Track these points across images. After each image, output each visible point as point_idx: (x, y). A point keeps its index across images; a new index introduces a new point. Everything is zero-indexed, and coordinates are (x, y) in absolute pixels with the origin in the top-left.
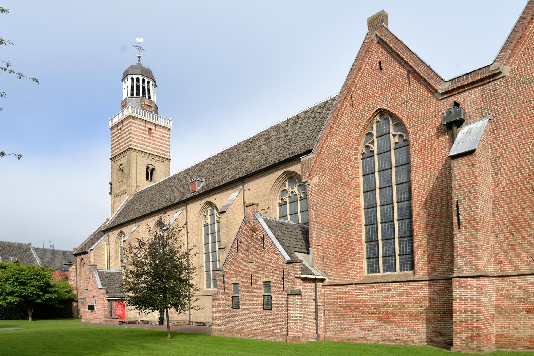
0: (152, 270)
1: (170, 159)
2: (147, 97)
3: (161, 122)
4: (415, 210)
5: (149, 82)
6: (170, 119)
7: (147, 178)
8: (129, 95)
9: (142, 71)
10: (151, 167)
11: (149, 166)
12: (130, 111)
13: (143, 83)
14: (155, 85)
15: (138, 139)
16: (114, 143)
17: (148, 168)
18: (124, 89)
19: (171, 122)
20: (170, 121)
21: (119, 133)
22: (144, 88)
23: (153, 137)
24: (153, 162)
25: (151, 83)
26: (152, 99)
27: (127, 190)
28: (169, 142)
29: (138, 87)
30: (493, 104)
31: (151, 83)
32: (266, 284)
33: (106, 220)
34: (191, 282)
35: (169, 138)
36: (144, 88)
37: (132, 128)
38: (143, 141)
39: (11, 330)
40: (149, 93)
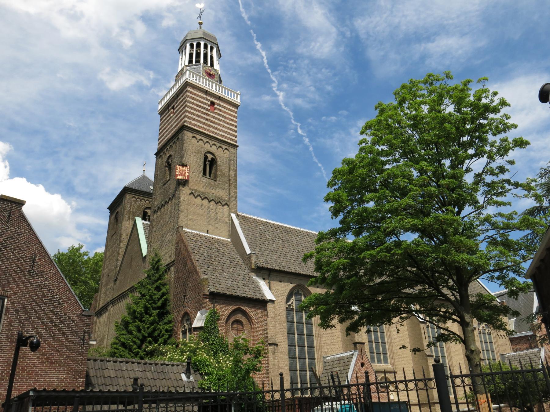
0: (434, 164)
1: (237, 146)
2: (209, 64)
4: (14, 342)
5: (212, 48)
6: (238, 92)
7: (205, 173)
8: (187, 63)
9: (203, 35)
10: (210, 157)
12: (187, 77)
13: (204, 48)
15: (197, 106)
16: (163, 122)
17: (206, 158)
18: (180, 60)
19: (239, 96)
22: (205, 55)
24: (213, 149)
25: (215, 51)
28: (236, 136)
29: (198, 55)
30: (20, 374)
31: (215, 51)
32: (290, 323)
36: (205, 55)
37: (187, 119)
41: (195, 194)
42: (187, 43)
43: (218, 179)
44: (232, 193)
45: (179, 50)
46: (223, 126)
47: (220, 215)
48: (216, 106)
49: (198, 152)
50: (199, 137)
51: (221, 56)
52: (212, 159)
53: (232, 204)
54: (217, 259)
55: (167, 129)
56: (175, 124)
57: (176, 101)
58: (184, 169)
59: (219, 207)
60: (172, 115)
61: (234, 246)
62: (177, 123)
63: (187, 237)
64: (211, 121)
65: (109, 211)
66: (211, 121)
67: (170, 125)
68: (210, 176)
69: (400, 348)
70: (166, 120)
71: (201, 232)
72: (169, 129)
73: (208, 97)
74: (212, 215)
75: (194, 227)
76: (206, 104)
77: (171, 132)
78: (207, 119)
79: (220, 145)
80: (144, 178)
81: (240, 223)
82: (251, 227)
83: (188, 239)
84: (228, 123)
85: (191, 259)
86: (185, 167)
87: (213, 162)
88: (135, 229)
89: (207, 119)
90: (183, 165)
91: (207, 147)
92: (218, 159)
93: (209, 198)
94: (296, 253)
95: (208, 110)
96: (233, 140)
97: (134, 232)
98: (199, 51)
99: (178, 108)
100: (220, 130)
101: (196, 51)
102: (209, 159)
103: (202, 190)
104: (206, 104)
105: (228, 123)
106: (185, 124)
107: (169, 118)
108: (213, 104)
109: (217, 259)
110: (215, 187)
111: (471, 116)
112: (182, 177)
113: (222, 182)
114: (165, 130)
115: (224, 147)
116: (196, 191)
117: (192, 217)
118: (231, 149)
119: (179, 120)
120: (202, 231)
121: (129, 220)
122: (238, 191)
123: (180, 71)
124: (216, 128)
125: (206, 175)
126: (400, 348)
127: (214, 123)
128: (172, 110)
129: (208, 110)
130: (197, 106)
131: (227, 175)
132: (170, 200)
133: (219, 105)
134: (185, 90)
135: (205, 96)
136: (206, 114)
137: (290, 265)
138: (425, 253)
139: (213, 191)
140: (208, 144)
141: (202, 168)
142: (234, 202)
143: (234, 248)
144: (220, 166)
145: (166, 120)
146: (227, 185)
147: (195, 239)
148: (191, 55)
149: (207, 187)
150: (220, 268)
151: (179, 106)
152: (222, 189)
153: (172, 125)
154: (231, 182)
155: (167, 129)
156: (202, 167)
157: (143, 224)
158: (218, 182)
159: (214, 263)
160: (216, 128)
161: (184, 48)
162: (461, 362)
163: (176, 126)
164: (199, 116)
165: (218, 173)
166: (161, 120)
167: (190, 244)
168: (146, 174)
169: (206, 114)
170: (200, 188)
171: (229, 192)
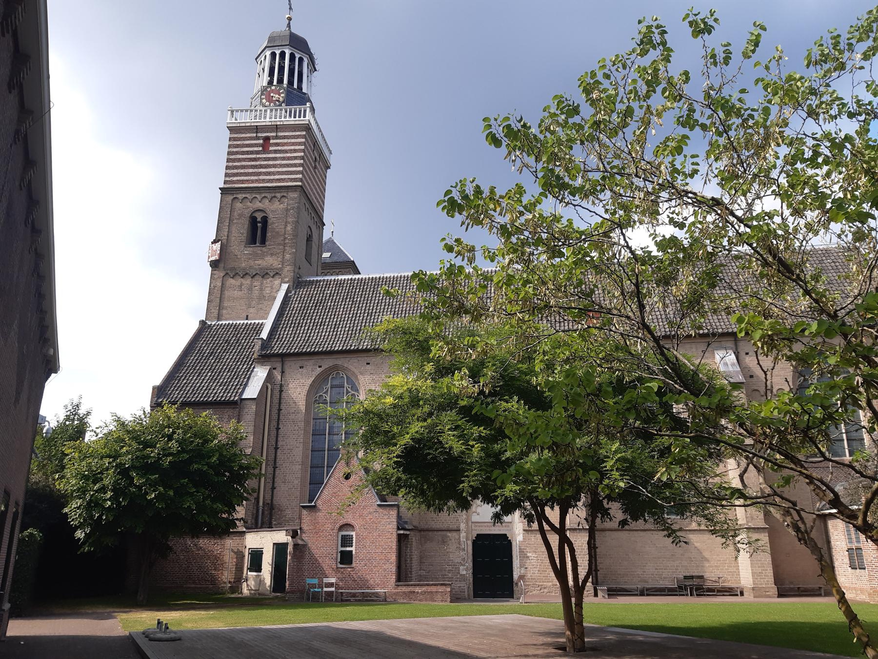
2: (295, 86)
10: (259, 216)
23: (315, 172)
27: (281, 269)
38: (320, 181)
43: (267, 243)
50: (241, 196)
69: (699, 13)
71: (235, 320)
92: (271, 216)
100: (273, 174)
110: (262, 256)
111: (130, 456)
115: (279, 195)
119: (242, 171)
120: (239, 319)
124: (269, 174)
126: (699, 13)
138: (774, 191)
139: (260, 262)
144: (273, 223)
152: (272, 255)
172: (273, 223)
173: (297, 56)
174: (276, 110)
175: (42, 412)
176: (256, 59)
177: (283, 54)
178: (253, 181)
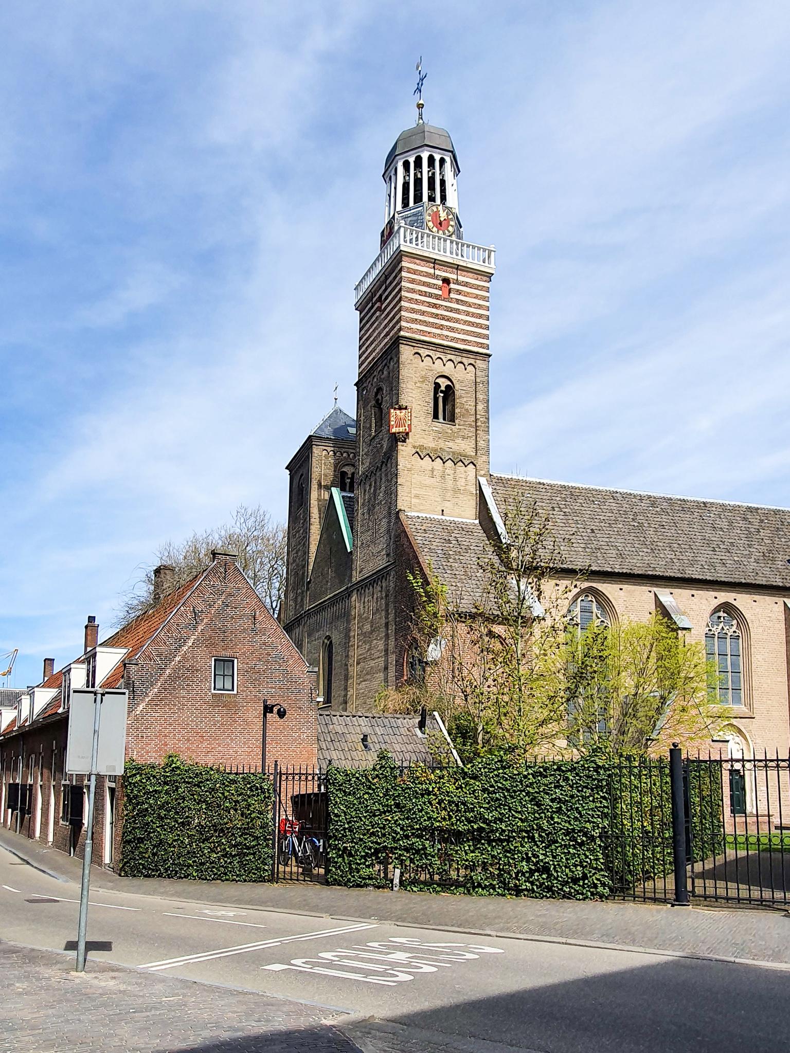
1: (489, 356)
3: (472, 260)
5: (442, 161)
7: (436, 416)
10: (443, 383)
11: (440, 381)
14: (457, 170)
15: (421, 293)
17: (437, 386)
20: (490, 251)
21: (379, 309)
22: (431, 180)
24: (448, 369)
25: (448, 165)
26: (449, 203)
28: (486, 337)
29: (418, 182)
33: (676, 907)
34: (120, 771)
35: (488, 309)
36: (431, 180)
39: (323, 671)
40: (443, 191)
41: (420, 453)
42: (397, 162)
43: (457, 421)
44: (481, 443)
45: (383, 176)
46: (465, 322)
47: (461, 483)
48: (452, 286)
49: (424, 379)
50: (424, 352)
51: (459, 171)
52: (447, 387)
53: (480, 462)
54: (457, 557)
55: (371, 339)
56: (385, 332)
57: (383, 287)
58: (402, 414)
59: (460, 468)
60: (378, 313)
61: (484, 532)
62: (387, 330)
63: (411, 526)
64: (443, 318)
65: (288, 472)
66: (443, 318)
67: (377, 332)
68: (444, 419)
70: (370, 323)
72: (374, 340)
73: (437, 272)
74: (450, 483)
75: (422, 508)
76: (434, 286)
77: (377, 345)
78: (436, 316)
79: (459, 359)
80: (338, 412)
81: (495, 492)
82: (513, 497)
83: (413, 530)
84: (473, 315)
85: (419, 563)
86: (404, 411)
87: (449, 392)
88: (331, 506)
89: (436, 316)
90: (400, 408)
91: (438, 367)
92: (457, 386)
93: (443, 457)
94: (585, 534)
95: (437, 297)
96: (482, 345)
97: (331, 506)
98: (419, 176)
99: (388, 301)
101: (415, 174)
102: (443, 388)
103: (432, 445)
104: (434, 286)
105: (473, 315)
106: (402, 333)
107: (374, 318)
108: (446, 281)
109: (457, 557)
112: (401, 429)
113: (463, 425)
114: (369, 342)
116: (421, 447)
117: (418, 492)
118: (480, 364)
119: (391, 325)
121: (321, 488)
122: (490, 437)
123: (388, 223)
124: (452, 329)
125: (438, 419)
127: (449, 319)
128: (378, 304)
129: (437, 297)
130: (421, 293)
131: (473, 412)
132: (384, 465)
133: (457, 282)
134: (399, 268)
135: (432, 271)
136: (435, 306)
137: (575, 556)
139: (450, 444)
140: (440, 360)
141: (431, 410)
142: (484, 458)
143: (485, 535)
144: (461, 397)
145: (370, 323)
146: (473, 430)
147: (423, 528)
148: (406, 186)
149: (439, 438)
150: (462, 573)
151: (390, 298)
152: (464, 438)
153: (380, 333)
154: (479, 424)
155: (371, 339)
156: (432, 405)
157: (343, 497)
158: (457, 426)
159: (453, 564)
160: (452, 329)
161: (393, 172)
162: (110, 976)
163: (386, 336)
164: (423, 313)
165: (457, 411)
166: (360, 348)
167: (416, 538)
168: (341, 405)
169: (435, 306)
170: (429, 443)
171: (476, 441)
172: (461, 397)
173: (437, 157)
174: (445, 240)
175: (401, 505)
176: (383, 176)
177: (418, 161)
178: (435, 336)
